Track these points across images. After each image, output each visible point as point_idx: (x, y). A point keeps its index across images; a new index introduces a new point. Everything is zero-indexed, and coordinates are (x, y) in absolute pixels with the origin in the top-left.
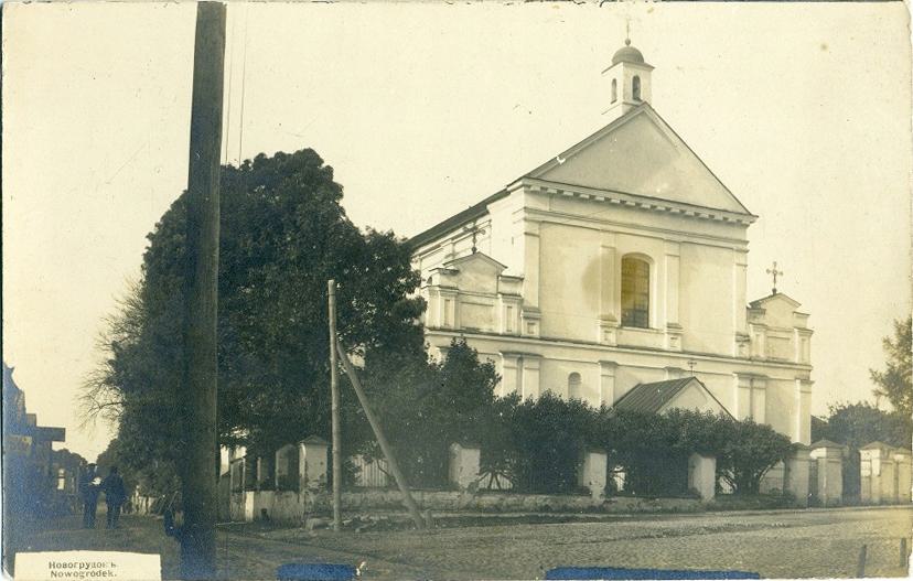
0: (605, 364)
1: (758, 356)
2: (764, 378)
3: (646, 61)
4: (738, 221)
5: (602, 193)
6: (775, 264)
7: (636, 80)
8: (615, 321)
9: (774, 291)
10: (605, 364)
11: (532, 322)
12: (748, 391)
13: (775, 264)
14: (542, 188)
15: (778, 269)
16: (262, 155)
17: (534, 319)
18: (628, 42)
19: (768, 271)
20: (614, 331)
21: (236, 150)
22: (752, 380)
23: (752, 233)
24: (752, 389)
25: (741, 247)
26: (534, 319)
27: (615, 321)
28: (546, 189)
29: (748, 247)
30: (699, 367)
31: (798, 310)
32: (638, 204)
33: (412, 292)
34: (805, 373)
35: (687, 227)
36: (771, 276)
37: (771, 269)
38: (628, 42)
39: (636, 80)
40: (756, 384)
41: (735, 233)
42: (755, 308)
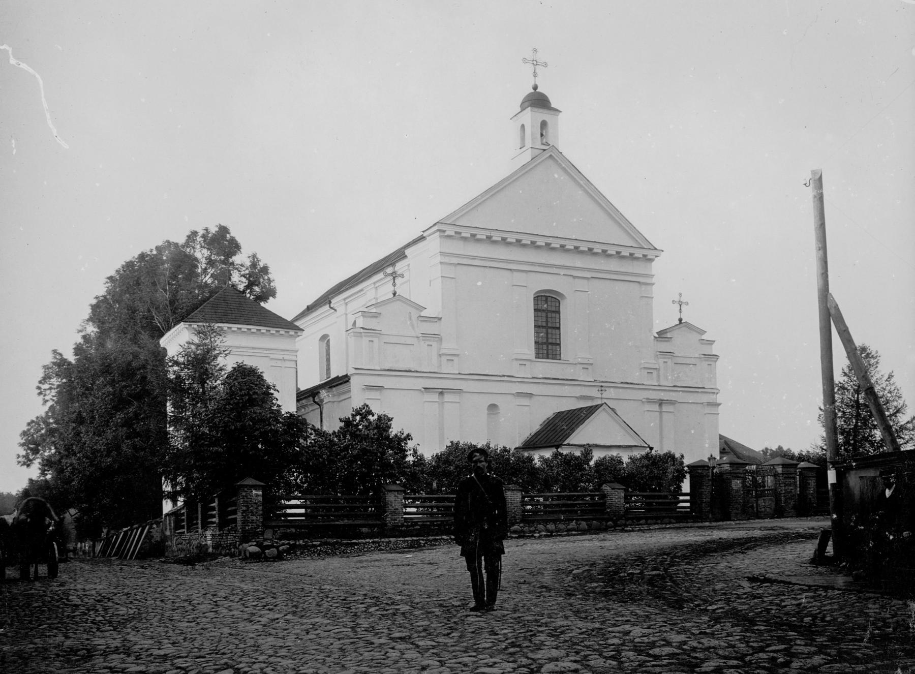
0: (520, 394)
2: (672, 403)
3: (553, 105)
4: (631, 254)
5: (598, 246)
7: (544, 124)
9: (680, 320)
10: (520, 394)
13: (680, 294)
18: (535, 88)
20: (528, 363)
22: (660, 405)
24: (661, 412)
25: (644, 282)
28: (279, 331)
29: (654, 280)
31: (704, 337)
37: (677, 299)
38: (535, 88)
39: (544, 124)
40: (665, 408)
42: (662, 335)
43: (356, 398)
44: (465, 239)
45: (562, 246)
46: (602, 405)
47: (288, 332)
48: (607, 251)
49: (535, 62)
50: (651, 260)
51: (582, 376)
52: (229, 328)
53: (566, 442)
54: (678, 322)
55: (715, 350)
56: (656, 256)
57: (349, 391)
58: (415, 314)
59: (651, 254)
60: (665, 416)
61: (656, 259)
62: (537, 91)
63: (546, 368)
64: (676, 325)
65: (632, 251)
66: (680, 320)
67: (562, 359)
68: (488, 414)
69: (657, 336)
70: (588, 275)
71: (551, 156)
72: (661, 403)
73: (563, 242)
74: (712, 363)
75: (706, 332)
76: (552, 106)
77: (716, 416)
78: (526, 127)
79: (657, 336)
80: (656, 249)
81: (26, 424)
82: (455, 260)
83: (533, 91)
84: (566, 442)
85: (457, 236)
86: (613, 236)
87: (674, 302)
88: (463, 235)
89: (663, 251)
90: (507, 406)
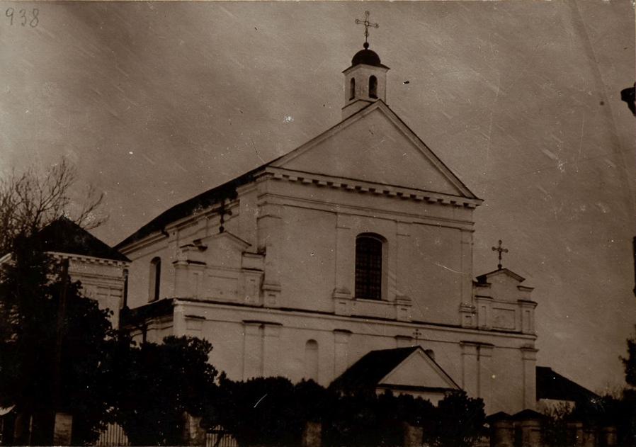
1: (349, 301)
2: (490, 346)
5: (308, 176)
6: (500, 242)
8: (350, 293)
9: (500, 266)
11: (273, 293)
13: (500, 242)
14: (105, 261)
15: (504, 246)
16: (207, 346)
17: (274, 291)
18: (366, 45)
19: (494, 249)
21: (161, 297)
22: (478, 349)
23: (476, 216)
25: (466, 229)
26: (274, 291)
27: (350, 293)
28: (107, 261)
30: (426, 334)
31: (522, 284)
32: (372, 190)
33: (553, 418)
34: (528, 342)
35: (424, 210)
36: (496, 254)
38: (366, 45)
40: (482, 351)
42: (482, 281)
43: (180, 328)
45: (440, 201)
46: (415, 348)
47: (107, 261)
48: (303, 179)
49: (367, 24)
50: (473, 208)
51: (400, 314)
52: (88, 259)
53: (380, 383)
54: (497, 269)
55: (533, 296)
56: (477, 205)
57: (172, 320)
58: (516, 283)
59: (472, 203)
61: (477, 207)
62: (369, 49)
63: (366, 307)
64: (496, 271)
65: (453, 199)
66: (500, 266)
67: (382, 298)
69: (477, 281)
71: (378, 108)
72: (478, 345)
73: (413, 192)
74: (531, 310)
75: (524, 279)
76: (381, 63)
77: (170, 329)
78: (356, 81)
79: (477, 281)
80: (476, 198)
81: (224, 369)
82: (411, 220)
83: (364, 49)
84: (380, 383)
85: (285, 179)
86: (435, 183)
87: (494, 249)
88: (291, 178)
89: (483, 200)
90: (325, 340)
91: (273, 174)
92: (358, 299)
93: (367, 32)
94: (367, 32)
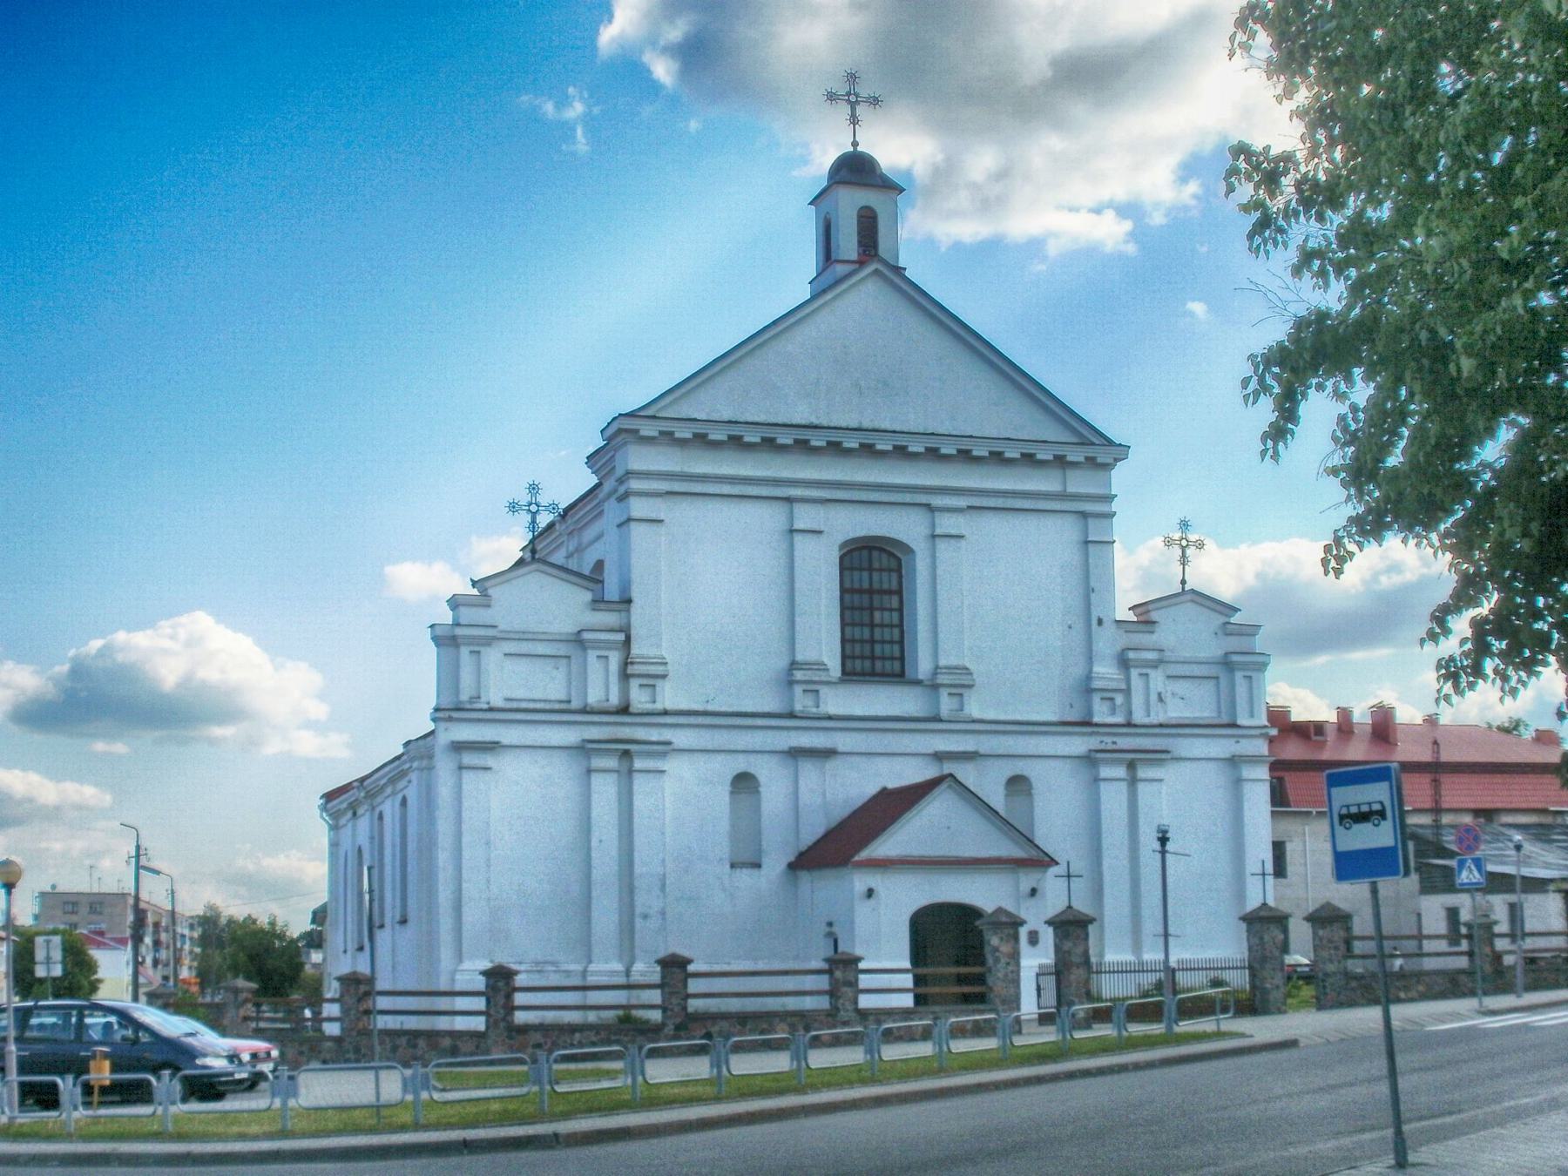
12: (1123, 786)
18: (855, 144)
29: (1115, 506)
41: (1079, 483)
44: (683, 443)
49: (853, 98)
60: (1141, 787)
68: (732, 793)
70: (962, 502)
84: (864, 854)
91: (637, 431)
92: (924, 668)
93: (1184, 555)
94: (1184, 555)
